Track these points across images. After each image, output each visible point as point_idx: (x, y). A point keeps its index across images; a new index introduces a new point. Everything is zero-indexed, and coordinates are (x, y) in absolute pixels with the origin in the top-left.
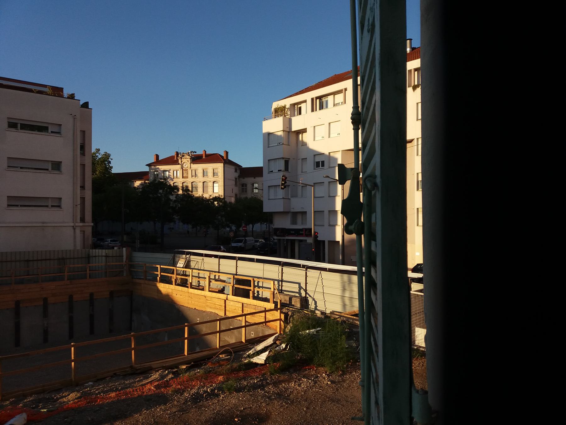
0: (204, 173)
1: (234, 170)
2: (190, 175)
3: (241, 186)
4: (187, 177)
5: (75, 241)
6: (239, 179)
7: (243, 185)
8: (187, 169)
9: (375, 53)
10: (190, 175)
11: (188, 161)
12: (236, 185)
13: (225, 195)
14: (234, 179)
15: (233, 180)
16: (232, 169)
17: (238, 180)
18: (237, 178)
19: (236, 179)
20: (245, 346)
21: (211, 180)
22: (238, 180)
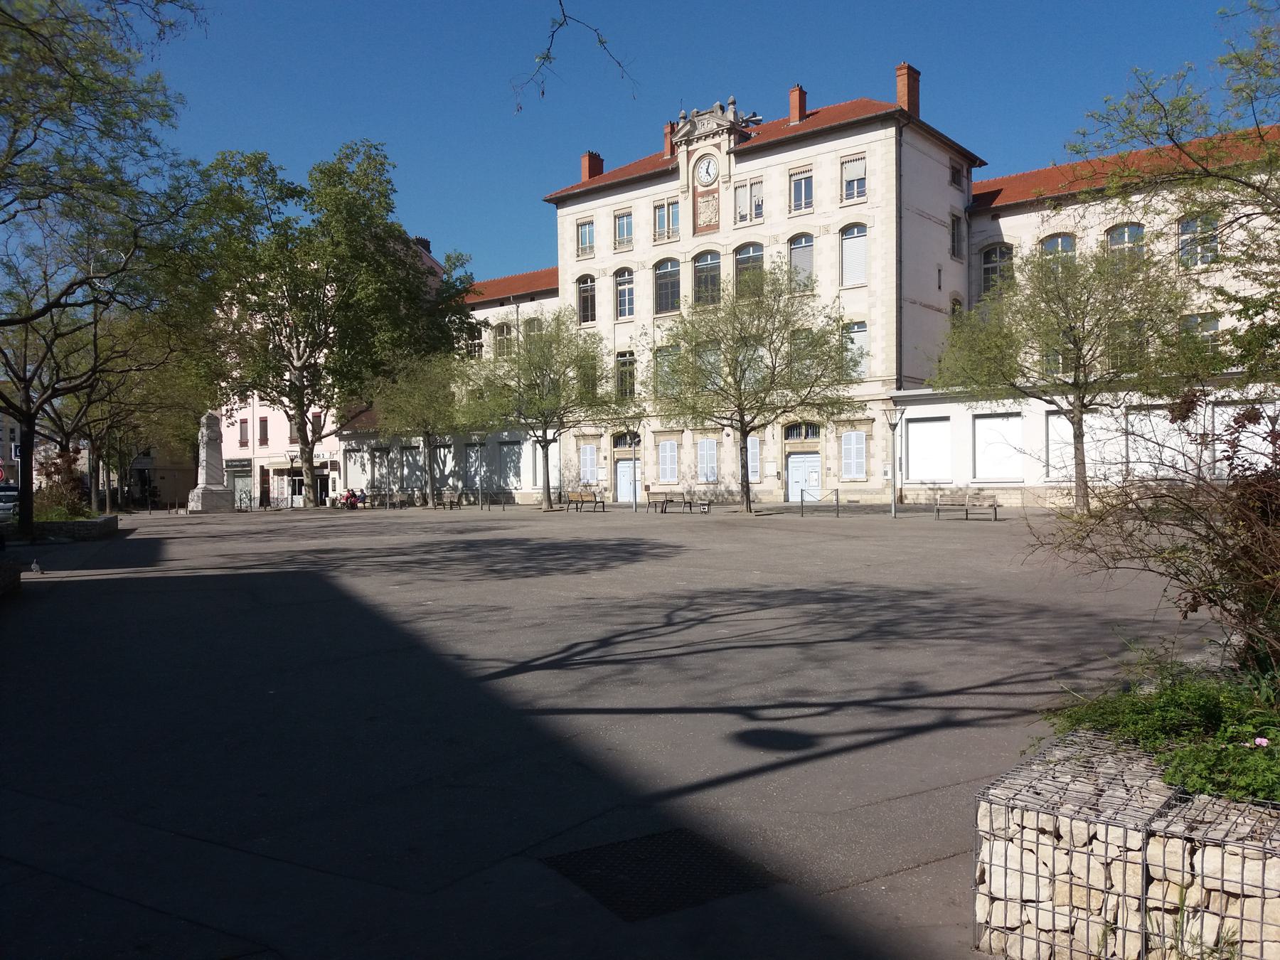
0: (802, 191)
1: (946, 174)
2: (727, 217)
3: (977, 260)
4: (713, 227)
5: (479, 669)
6: (969, 226)
7: (988, 254)
8: (715, 186)
9: (1027, 715)
10: (727, 217)
11: (718, 146)
12: (955, 252)
13: (905, 373)
14: (948, 220)
15: (942, 224)
16: (938, 165)
17: (964, 227)
18: (961, 214)
19: (956, 221)
20: (640, 656)
21: (826, 222)
22: (964, 227)
